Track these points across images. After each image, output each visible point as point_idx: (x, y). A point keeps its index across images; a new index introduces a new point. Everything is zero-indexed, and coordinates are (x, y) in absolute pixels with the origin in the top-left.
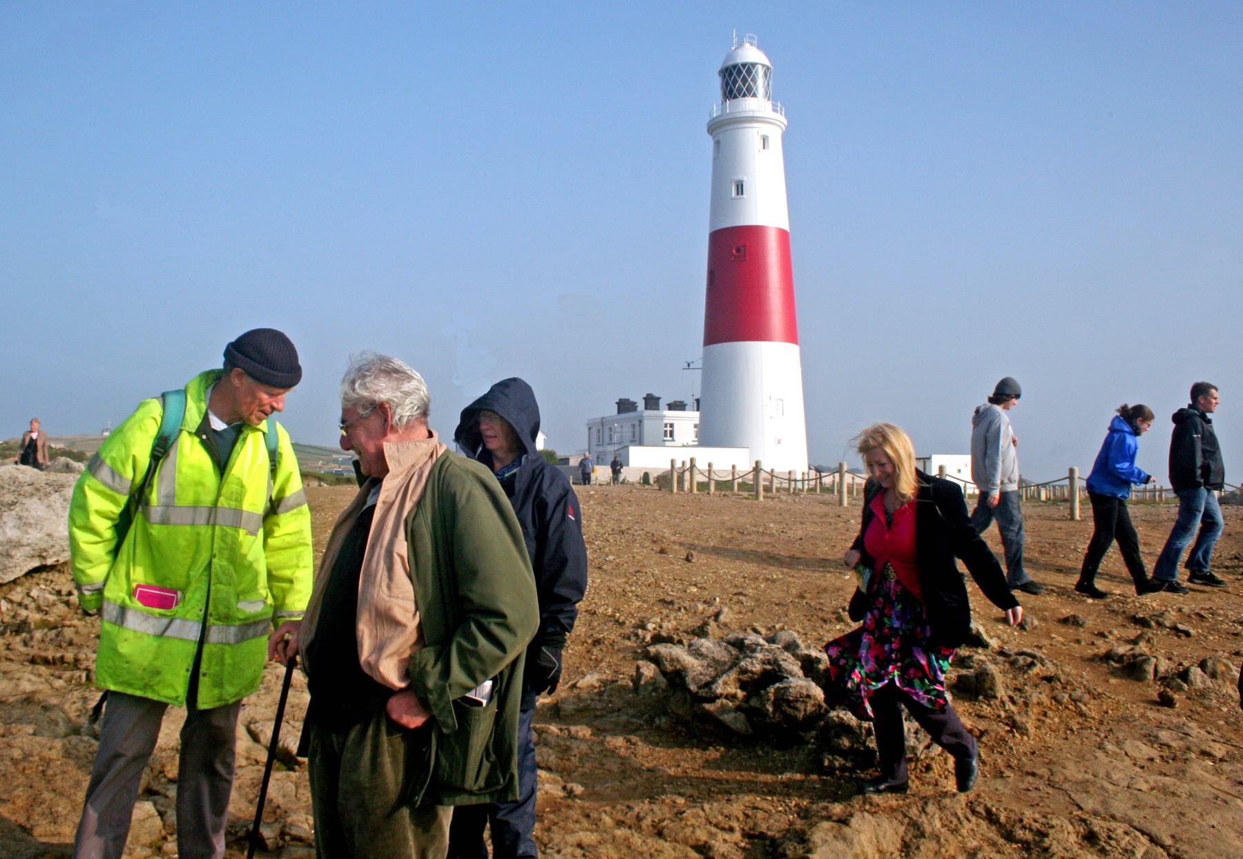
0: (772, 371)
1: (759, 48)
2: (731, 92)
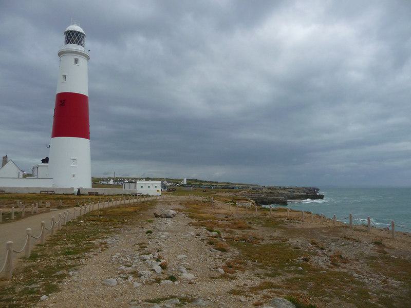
2: (69, 41)
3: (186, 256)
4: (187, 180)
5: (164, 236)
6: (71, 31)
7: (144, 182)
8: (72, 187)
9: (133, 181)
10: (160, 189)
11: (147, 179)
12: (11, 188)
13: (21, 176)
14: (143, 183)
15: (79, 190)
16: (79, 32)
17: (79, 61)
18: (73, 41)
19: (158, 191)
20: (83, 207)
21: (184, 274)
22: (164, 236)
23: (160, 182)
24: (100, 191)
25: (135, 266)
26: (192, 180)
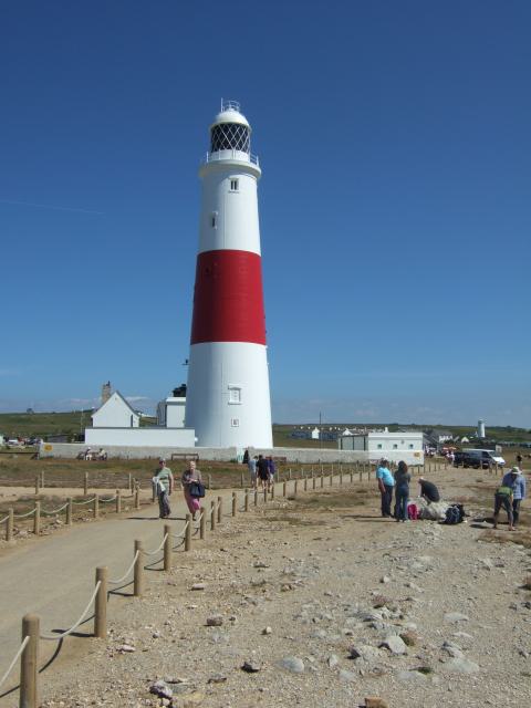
0: (247, 366)
1: (241, 112)
2: (219, 144)
3: (466, 617)
4: (486, 428)
5: (419, 565)
6: (222, 125)
7: (386, 433)
8: (234, 445)
9: (363, 430)
10: (421, 452)
11: (394, 428)
12: (118, 448)
13: (136, 424)
14: (381, 439)
15: (247, 453)
16: (238, 125)
17: (240, 184)
18: (241, 145)
19: (417, 455)
20: (318, 480)
21: (454, 660)
22: (419, 565)
23: (420, 435)
24: (291, 453)
25: (347, 631)
26: (498, 428)
